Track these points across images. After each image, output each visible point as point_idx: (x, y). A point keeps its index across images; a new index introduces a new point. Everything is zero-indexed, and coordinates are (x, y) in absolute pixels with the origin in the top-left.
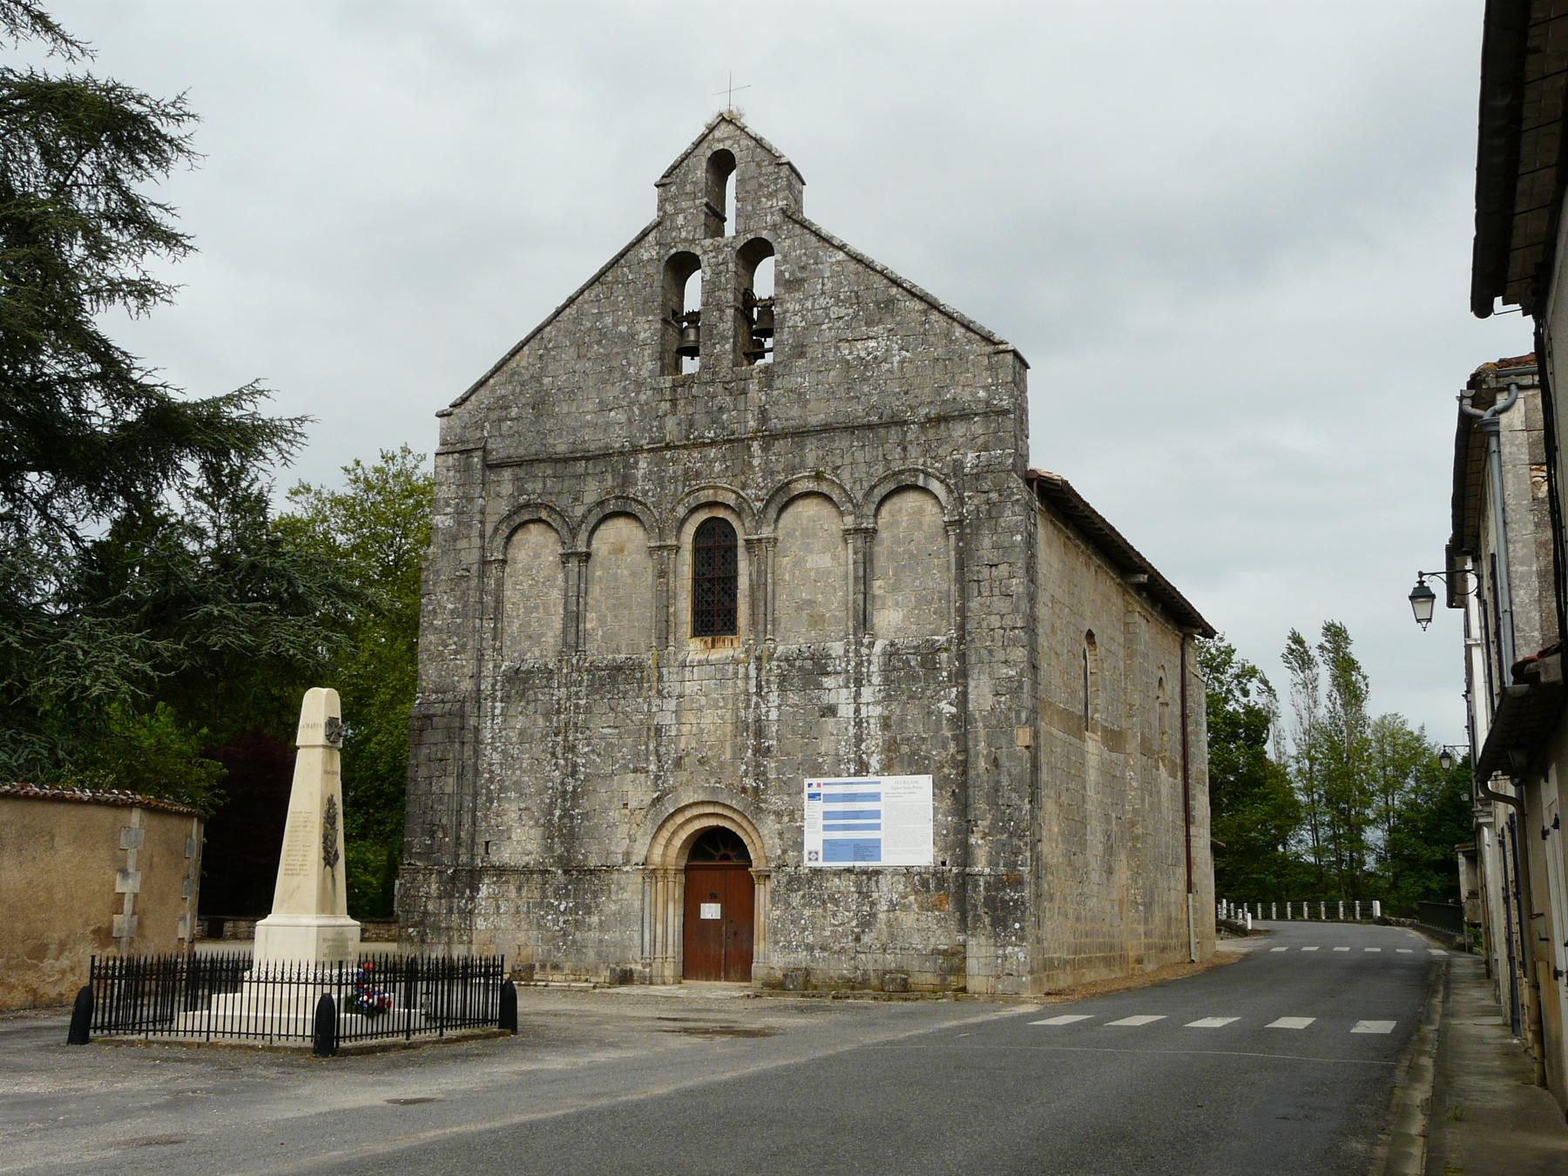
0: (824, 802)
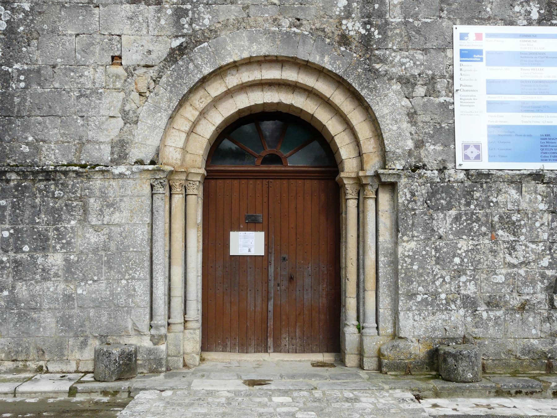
0: (487, 65)
